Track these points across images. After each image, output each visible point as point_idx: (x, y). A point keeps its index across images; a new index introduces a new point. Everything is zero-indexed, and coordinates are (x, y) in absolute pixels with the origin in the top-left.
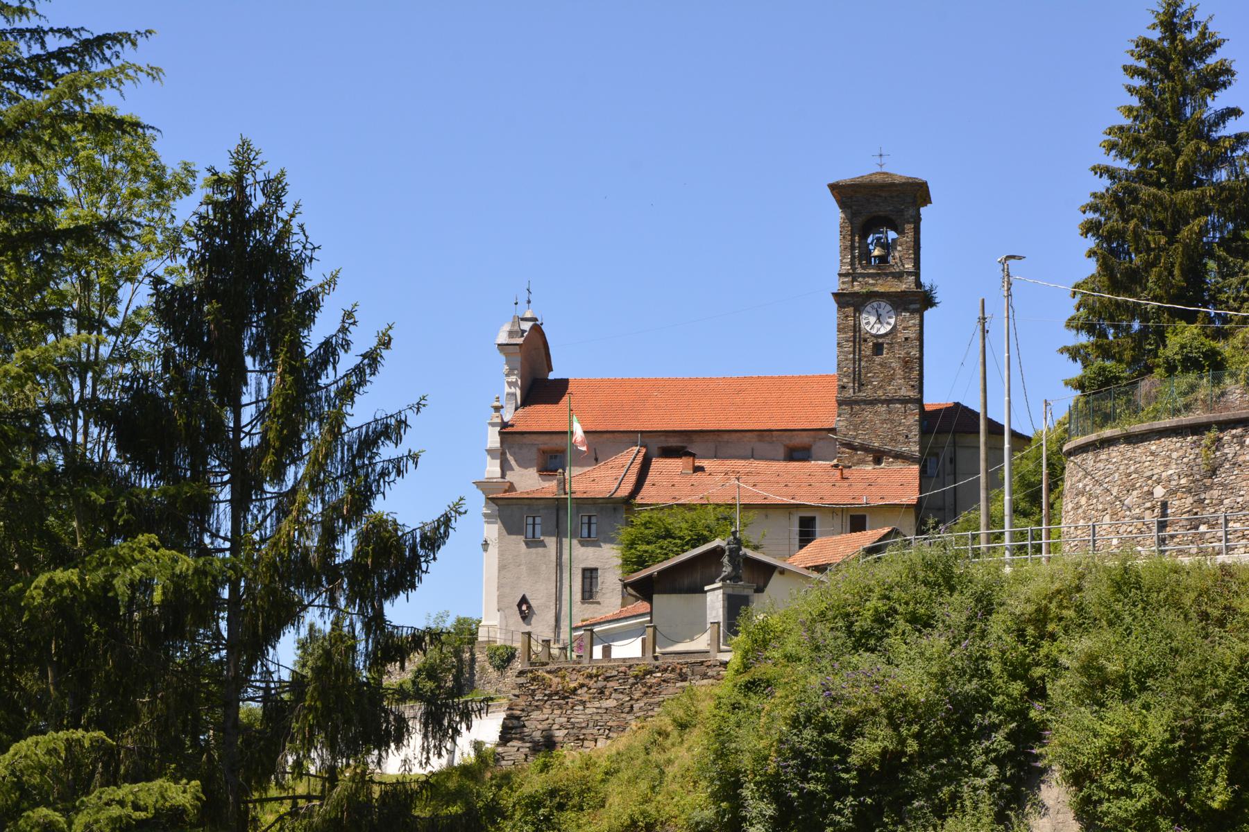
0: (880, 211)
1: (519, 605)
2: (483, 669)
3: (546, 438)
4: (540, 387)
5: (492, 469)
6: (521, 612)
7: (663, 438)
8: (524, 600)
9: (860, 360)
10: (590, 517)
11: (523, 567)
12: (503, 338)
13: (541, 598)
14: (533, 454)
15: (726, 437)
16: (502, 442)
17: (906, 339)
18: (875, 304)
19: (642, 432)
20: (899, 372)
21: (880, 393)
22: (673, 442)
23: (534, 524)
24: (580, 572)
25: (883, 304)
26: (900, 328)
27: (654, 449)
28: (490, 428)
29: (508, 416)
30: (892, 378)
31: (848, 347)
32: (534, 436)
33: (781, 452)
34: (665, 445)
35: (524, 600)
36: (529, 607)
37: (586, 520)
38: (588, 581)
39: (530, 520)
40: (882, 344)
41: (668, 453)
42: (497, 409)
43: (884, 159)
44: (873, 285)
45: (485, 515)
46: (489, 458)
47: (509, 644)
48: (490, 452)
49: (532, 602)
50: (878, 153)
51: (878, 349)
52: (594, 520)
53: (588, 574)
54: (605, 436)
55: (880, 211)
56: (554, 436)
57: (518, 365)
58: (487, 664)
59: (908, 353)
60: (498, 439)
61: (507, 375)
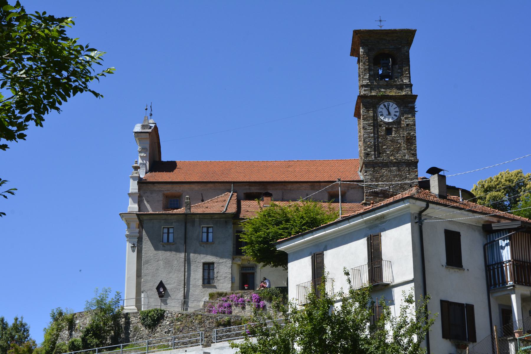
0: (385, 54)
1: (158, 289)
2: (136, 329)
3: (169, 186)
4: (157, 164)
5: (133, 207)
6: (160, 293)
7: (247, 187)
8: (161, 285)
9: (378, 138)
10: (208, 228)
11: (161, 262)
12: (138, 128)
13: (174, 283)
14: (160, 197)
15: (290, 186)
16: (139, 189)
17: (407, 125)
18: (386, 104)
19: (234, 183)
20: (404, 145)
21: (392, 158)
22: (254, 190)
23: (168, 233)
24: (201, 265)
25: (391, 104)
26: (403, 118)
27: (242, 196)
28: (131, 181)
29: (142, 174)
30: (399, 149)
31: (370, 129)
32: (161, 185)
33: (326, 196)
34: (248, 191)
35: (161, 285)
36: (165, 289)
37: (205, 230)
38: (207, 271)
39: (166, 231)
40: (391, 128)
41: (250, 197)
42: (136, 168)
43: (382, 23)
44: (385, 92)
45: (127, 236)
46: (130, 200)
47: (159, 308)
48: (130, 195)
49: (166, 286)
50: (379, 19)
51: (389, 131)
52: (210, 230)
53: (206, 266)
54: (209, 185)
55: (385, 54)
56: (175, 185)
57: (148, 146)
58: (140, 325)
59: (409, 134)
60: (136, 187)
61: (140, 152)
